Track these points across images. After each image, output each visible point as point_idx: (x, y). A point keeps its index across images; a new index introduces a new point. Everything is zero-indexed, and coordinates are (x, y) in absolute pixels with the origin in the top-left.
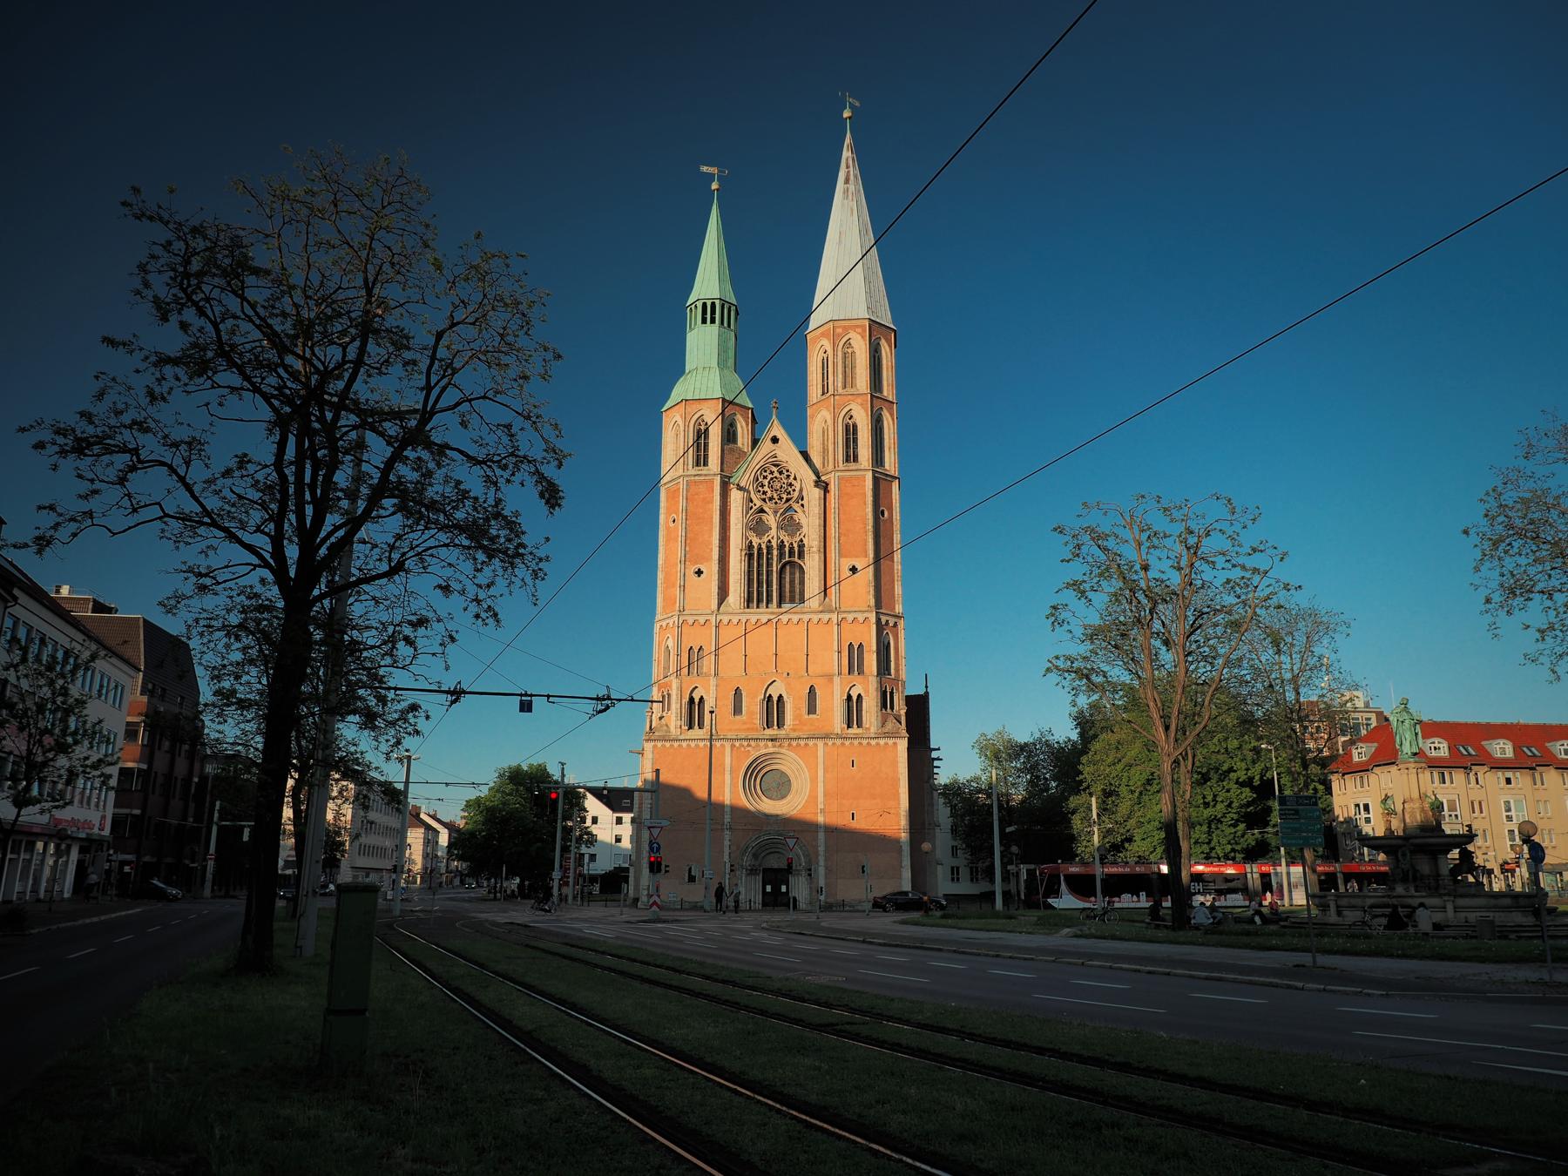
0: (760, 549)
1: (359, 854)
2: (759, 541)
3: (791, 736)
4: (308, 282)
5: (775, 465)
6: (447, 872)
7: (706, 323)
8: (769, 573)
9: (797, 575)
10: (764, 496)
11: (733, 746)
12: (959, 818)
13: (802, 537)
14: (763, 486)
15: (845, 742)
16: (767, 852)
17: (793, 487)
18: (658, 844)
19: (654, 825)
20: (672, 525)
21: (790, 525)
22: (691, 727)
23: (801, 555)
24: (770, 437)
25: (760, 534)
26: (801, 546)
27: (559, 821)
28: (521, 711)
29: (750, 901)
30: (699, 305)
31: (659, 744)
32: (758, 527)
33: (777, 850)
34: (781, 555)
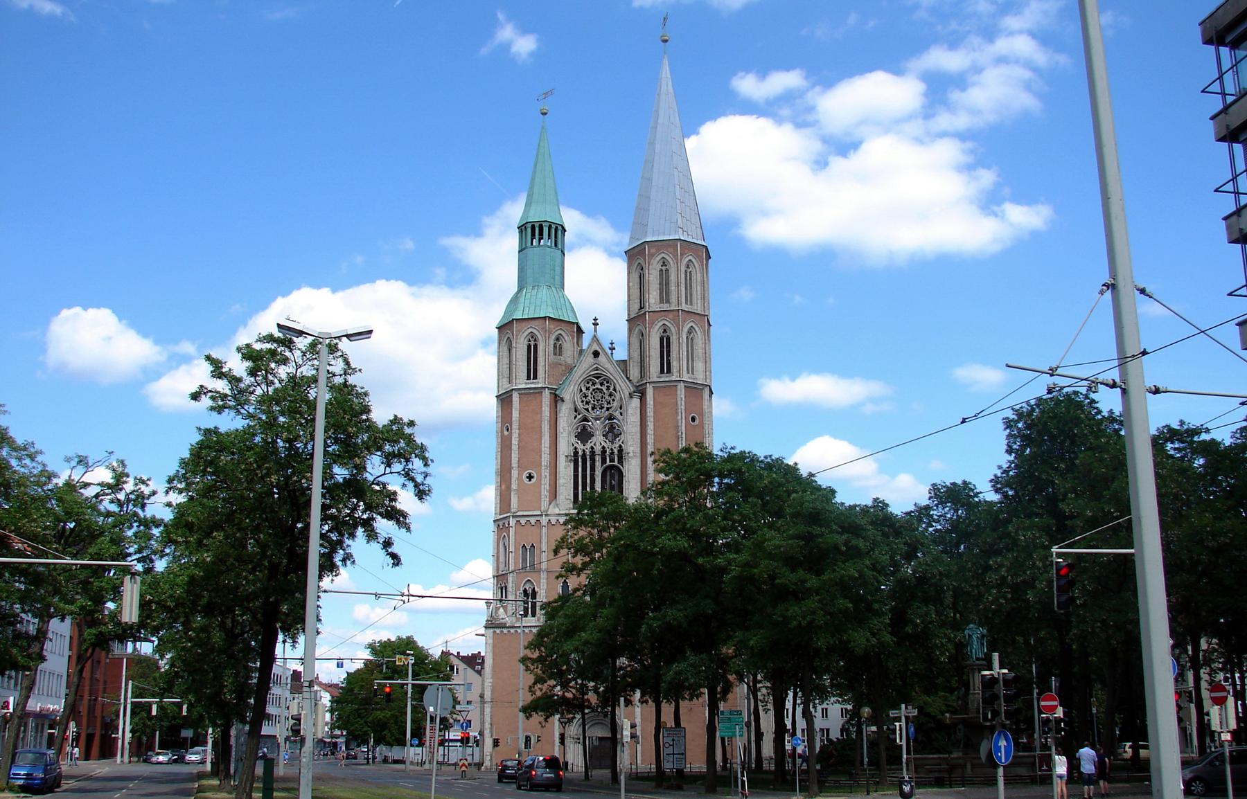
0: (584, 455)
1: (281, 676)
2: (582, 447)
4: (523, 227)
5: (597, 378)
12: (766, 700)
13: (620, 443)
14: (594, 384)
16: (597, 721)
17: (613, 397)
19: (463, 709)
20: (506, 433)
21: (613, 432)
22: (526, 615)
24: (592, 352)
25: (584, 442)
26: (621, 450)
27: (530, 606)
28: (625, 252)
30: (529, 226)
31: (498, 631)
32: (584, 435)
34: (604, 461)
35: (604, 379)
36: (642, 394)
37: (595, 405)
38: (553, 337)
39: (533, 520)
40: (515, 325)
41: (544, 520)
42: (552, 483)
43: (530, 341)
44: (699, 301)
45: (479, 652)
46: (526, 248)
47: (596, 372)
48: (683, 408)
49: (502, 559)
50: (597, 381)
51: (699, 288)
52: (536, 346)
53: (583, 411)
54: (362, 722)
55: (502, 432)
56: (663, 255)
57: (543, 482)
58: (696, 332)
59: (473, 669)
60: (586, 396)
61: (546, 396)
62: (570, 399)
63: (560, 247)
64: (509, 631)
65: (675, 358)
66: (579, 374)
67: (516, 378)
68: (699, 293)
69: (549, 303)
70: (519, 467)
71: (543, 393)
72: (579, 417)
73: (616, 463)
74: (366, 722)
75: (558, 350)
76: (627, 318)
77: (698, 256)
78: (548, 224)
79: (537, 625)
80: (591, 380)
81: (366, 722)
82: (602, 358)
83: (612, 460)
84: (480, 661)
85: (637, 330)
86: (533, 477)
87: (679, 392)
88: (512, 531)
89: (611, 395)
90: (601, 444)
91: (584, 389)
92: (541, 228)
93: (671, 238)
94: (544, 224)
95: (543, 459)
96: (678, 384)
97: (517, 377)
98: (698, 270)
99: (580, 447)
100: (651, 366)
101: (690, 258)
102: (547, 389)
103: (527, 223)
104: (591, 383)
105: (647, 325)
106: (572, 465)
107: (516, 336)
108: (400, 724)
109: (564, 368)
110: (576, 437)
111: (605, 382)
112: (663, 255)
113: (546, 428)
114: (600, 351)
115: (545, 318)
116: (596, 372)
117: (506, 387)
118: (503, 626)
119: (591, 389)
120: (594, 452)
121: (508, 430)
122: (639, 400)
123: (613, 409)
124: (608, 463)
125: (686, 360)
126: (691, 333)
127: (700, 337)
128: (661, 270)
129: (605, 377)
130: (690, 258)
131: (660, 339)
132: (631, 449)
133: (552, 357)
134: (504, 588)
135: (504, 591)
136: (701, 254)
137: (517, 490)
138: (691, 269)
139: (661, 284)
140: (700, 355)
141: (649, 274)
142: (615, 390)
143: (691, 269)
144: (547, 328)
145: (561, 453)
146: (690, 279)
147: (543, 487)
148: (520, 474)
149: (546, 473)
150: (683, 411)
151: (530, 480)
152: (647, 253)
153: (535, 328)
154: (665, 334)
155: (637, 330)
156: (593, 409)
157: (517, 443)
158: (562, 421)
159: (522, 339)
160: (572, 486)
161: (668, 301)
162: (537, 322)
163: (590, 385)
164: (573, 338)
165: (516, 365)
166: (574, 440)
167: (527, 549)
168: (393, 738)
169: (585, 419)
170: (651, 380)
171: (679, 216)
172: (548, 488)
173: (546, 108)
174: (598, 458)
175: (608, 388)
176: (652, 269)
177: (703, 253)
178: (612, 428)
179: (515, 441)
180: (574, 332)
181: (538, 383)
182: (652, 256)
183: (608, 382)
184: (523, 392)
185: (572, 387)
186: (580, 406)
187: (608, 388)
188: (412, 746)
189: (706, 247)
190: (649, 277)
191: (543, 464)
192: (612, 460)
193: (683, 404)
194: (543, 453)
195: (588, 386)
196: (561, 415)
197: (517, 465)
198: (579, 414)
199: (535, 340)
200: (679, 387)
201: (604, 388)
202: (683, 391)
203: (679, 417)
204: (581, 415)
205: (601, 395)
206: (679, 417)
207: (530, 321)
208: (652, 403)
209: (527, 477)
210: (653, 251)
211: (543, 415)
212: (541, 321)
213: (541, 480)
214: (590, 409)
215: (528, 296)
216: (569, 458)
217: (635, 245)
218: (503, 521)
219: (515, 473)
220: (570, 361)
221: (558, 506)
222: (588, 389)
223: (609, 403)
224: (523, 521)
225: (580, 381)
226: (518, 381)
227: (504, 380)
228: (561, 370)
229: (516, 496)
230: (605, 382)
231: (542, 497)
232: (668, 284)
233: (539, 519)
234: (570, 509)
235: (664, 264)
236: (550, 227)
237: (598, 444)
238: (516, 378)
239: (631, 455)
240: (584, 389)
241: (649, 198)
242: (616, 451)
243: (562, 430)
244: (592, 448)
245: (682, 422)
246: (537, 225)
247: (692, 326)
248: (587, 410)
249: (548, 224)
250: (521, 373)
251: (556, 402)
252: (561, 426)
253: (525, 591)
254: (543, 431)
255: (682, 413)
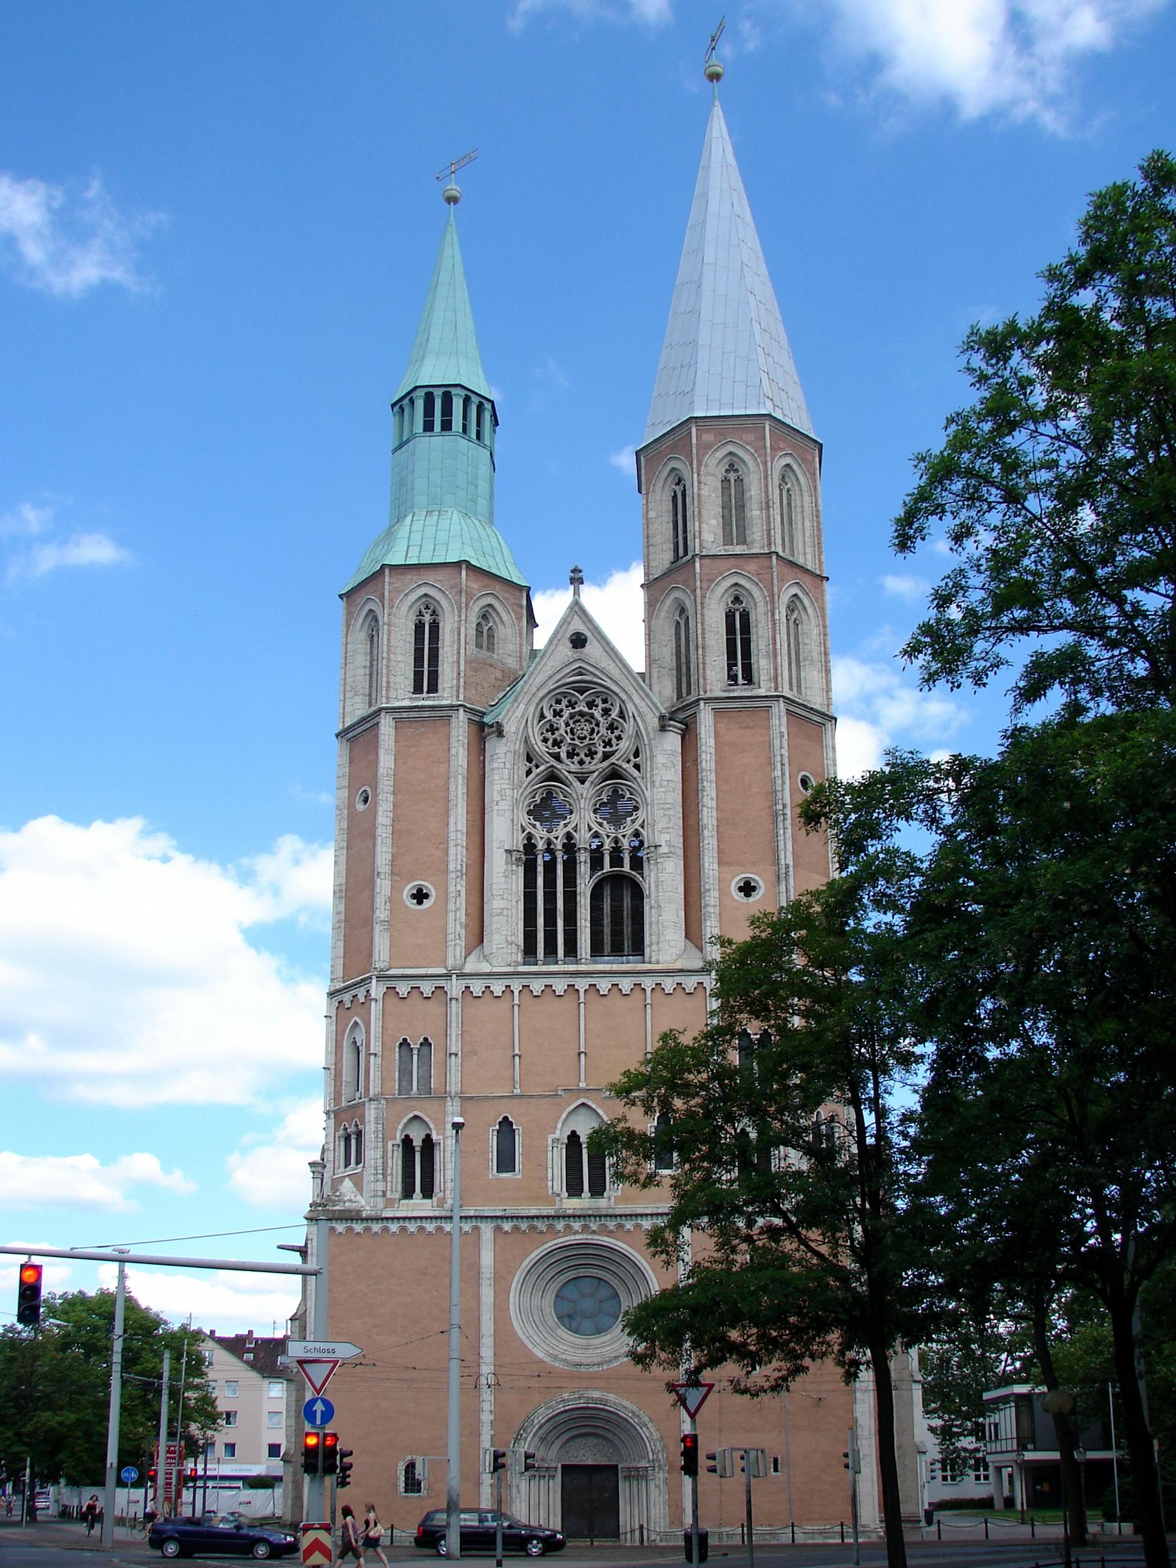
0: (550, 850)
3: (385, 1214)
4: (406, 401)
5: (582, 691)
6: (325, 1434)
7: (432, 430)
8: (571, 898)
9: (627, 902)
10: (556, 750)
11: (498, 1229)
15: (608, 1223)
17: (617, 733)
18: (326, 1403)
20: (360, 807)
22: (408, 1193)
23: (637, 864)
29: (641, 1527)
30: (421, 393)
31: (340, 1227)
33: (605, 1433)
35: (597, 694)
36: (686, 725)
37: (574, 747)
38: (476, 608)
39: (427, 988)
40: (387, 579)
41: (455, 987)
42: (475, 911)
43: (421, 614)
44: (809, 550)
45: (251, 1332)
46: (413, 437)
47: (579, 678)
48: (785, 752)
49: (347, 1074)
50: (581, 698)
51: (807, 524)
52: (435, 627)
53: (547, 757)
54: (10, 1433)
55: (351, 806)
56: (731, 448)
57: (451, 906)
58: (804, 608)
59: (240, 1357)
60: (552, 729)
61: (460, 725)
62: (516, 733)
63: (487, 442)
64: (367, 1229)
65: (763, 652)
66: (541, 679)
67: (388, 688)
68: (808, 533)
69: (467, 539)
70: (393, 873)
71: (453, 720)
72: (535, 771)
73: (627, 868)
74: (18, 1435)
75: (485, 635)
76: (642, 582)
77: (804, 460)
78: (463, 393)
79: (437, 1214)
80: (565, 695)
81: (18, 1435)
82: (592, 649)
83: (617, 860)
84: (253, 1346)
85: (669, 601)
86: (427, 896)
87: (775, 721)
88: (375, 1009)
89: (611, 728)
90: (590, 829)
91: (549, 715)
92: (447, 399)
93: (748, 413)
94: (454, 391)
95: (452, 858)
96: (774, 704)
97: (392, 685)
98: (804, 489)
99: (540, 834)
100: (708, 667)
101: (788, 460)
102: (461, 710)
103: (416, 388)
104: (565, 702)
105: (698, 583)
106: (521, 871)
107: (391, 600)
108: (95, 1438)
109: (499, 675)
110: (529, 813)
111: (599, 701)
112: (731, 448)
113: (459, 791)
114: (588, 634)
115: (458, 565)
116: (579, 678)
117: (358, 709)
118: (352, 1216)
119: (566, 714)
120: (574, 845)
121: (366, 800)
122: (680, 737)
123: (617, 755)
124: (607, 867)
125: (787, 658)
126: (793, 611)
127: (813, 623)
128: (726, 480)
129: (600, 689)
130: (788, 460)
131: (727, 616)
132: (662, 839)
133: (472, 646)
134: (353, 1136)
135: (353, 1142)
136: (810, 458)
137: (389, 924)
138: (789, 486)
139: (725, 506)
140: (815, 655)
141: (699, 482)
142: (622, 715)
143: (789, 486)
144: (464, 586)
145: (496, 844)
146: (789, 505)
147: (451, 916)
148: (396, 888)
149: (458, 887)
150: (786, 761)
151: (420, 903)
152: (694, 441)
153: (437, 588)
154: (737, 606)
155: (669, 601)
156: (570, 755)
157: (389, 822)
158: (496, 777)
159: (404, 608)
160: (521, 916)
161: (743, 541)
162: (441, 574)
163: (563, 706)
164: (519, 619)
165: (389, 660)
166: (524, 819)
167: (411, 1050)
168: (80, 1468)
169: (552, 776)
170: (708, 695)
171: (764, 377)
172: (463, 919)
173: (454, 188)
174: (583, 857)
175: (606, 712)
176: (708, 474)
177: (814, 458)
178: (616, 795)
179: (384, 818)
180: (521, 607)
181: (442, 698)
182: (705, 448)
183: (605, 701)
184: (405, 715)
185: (522, 707)
186: (541, 748)
187: (606, 712)
188: (121, 1483)
189: (821, 445)
190: (699, 489)
191: (452, 866)
192: (617, 860)
193: (785, 744)
194: (451, 844)
195: (558, 707)
196: (495, 765)
197: (388, 869)
198: (537, 767)
199: (434, 613)
200: (775, 710)
201: (597, 713)
202: (784, 719)
203: (778, 773)
204: (542, 768)
205: (588, 727)
206: (778, 773)
207: (422, 571)
208: (712, 742)
209: (414, 896)
210: (708, 437)
211: (452, 763)
212: (448, 571)
213: (447, 900)
214: (563, 756)
215: (418, 525)
216: (515, 855)
217: (664, 432)
218: (353, 992)
219: (383, 886)
220: (512, 663)
221: (486, 958)
222: (558, 714)
223: (608, 743)
224: (403, 988)
225: (541, 695)
226: (393, 694)
227: (358, 699)
228: (492, 676)
229: (387, 935)
230: (599, 701)
231: (451, 937)
232: (741, 507)
233: (441, 983)
234: (517, 964)
235: (731, 468)
236: (467, 400)
237: (583, 828)
238: (388, 688)
239: (664, 849)
240: (549, 715)
241: (695, 343)
242: (625, 844)
243: (497, 797)
244: (569, 836)
245: (783, 782)
246: (438, 393)
247: (795, 595)
248: (557, 757)
249: (463, 393)
250: (400, 679)
251: (482, 740)
252: (497, 788)
253: (407, 1142)
254: (451, 797)
255: (783, 765)
